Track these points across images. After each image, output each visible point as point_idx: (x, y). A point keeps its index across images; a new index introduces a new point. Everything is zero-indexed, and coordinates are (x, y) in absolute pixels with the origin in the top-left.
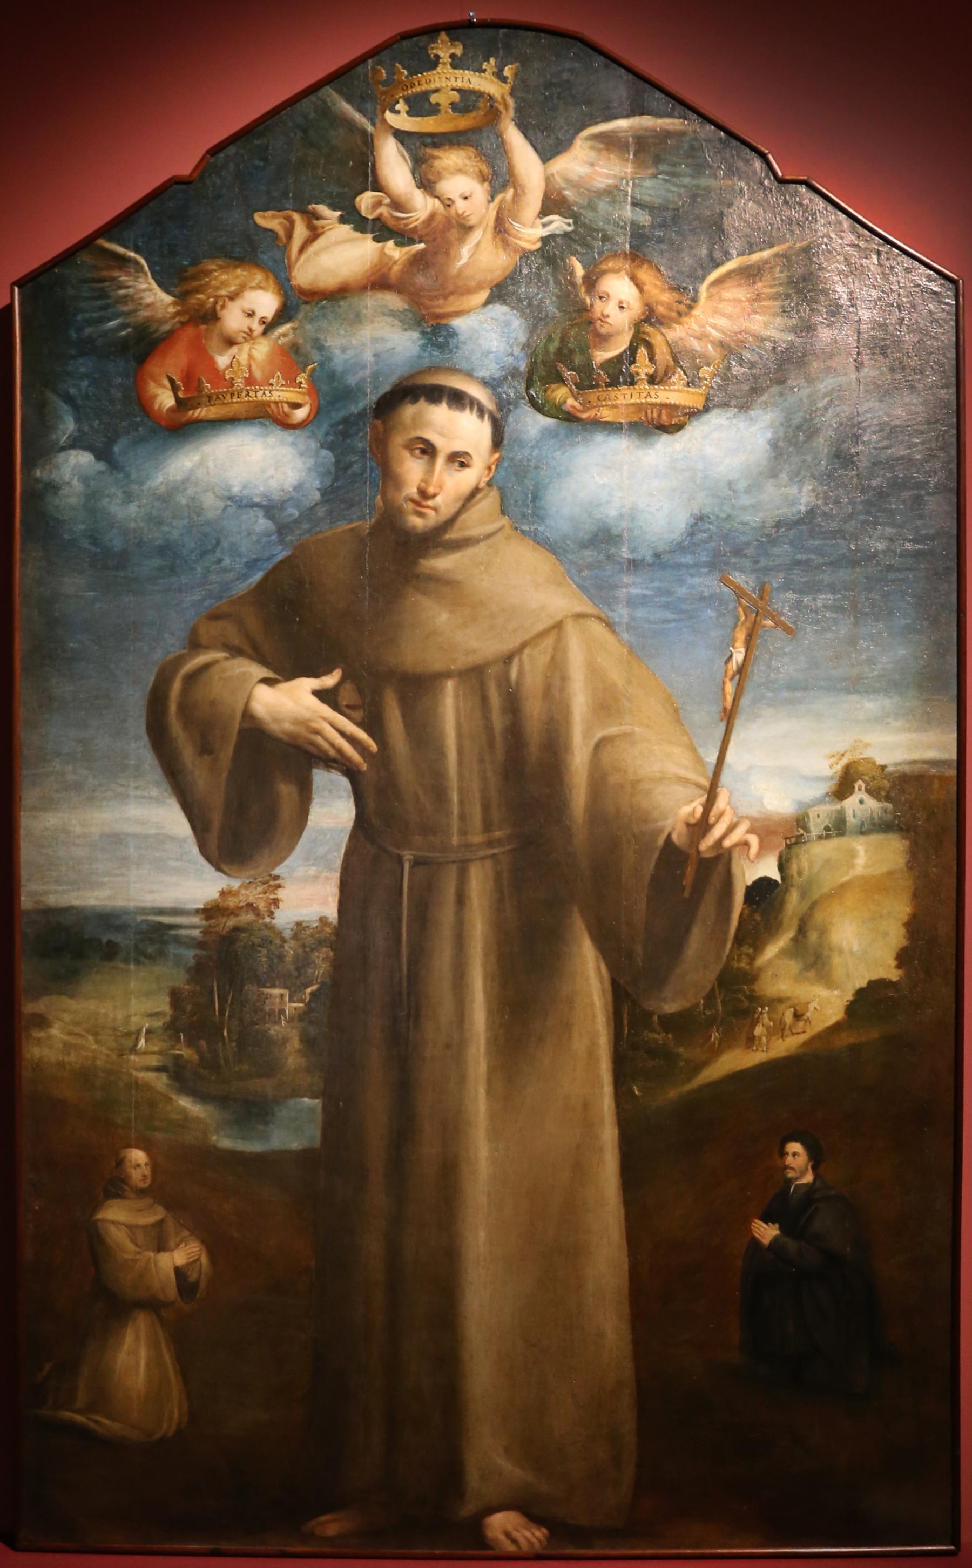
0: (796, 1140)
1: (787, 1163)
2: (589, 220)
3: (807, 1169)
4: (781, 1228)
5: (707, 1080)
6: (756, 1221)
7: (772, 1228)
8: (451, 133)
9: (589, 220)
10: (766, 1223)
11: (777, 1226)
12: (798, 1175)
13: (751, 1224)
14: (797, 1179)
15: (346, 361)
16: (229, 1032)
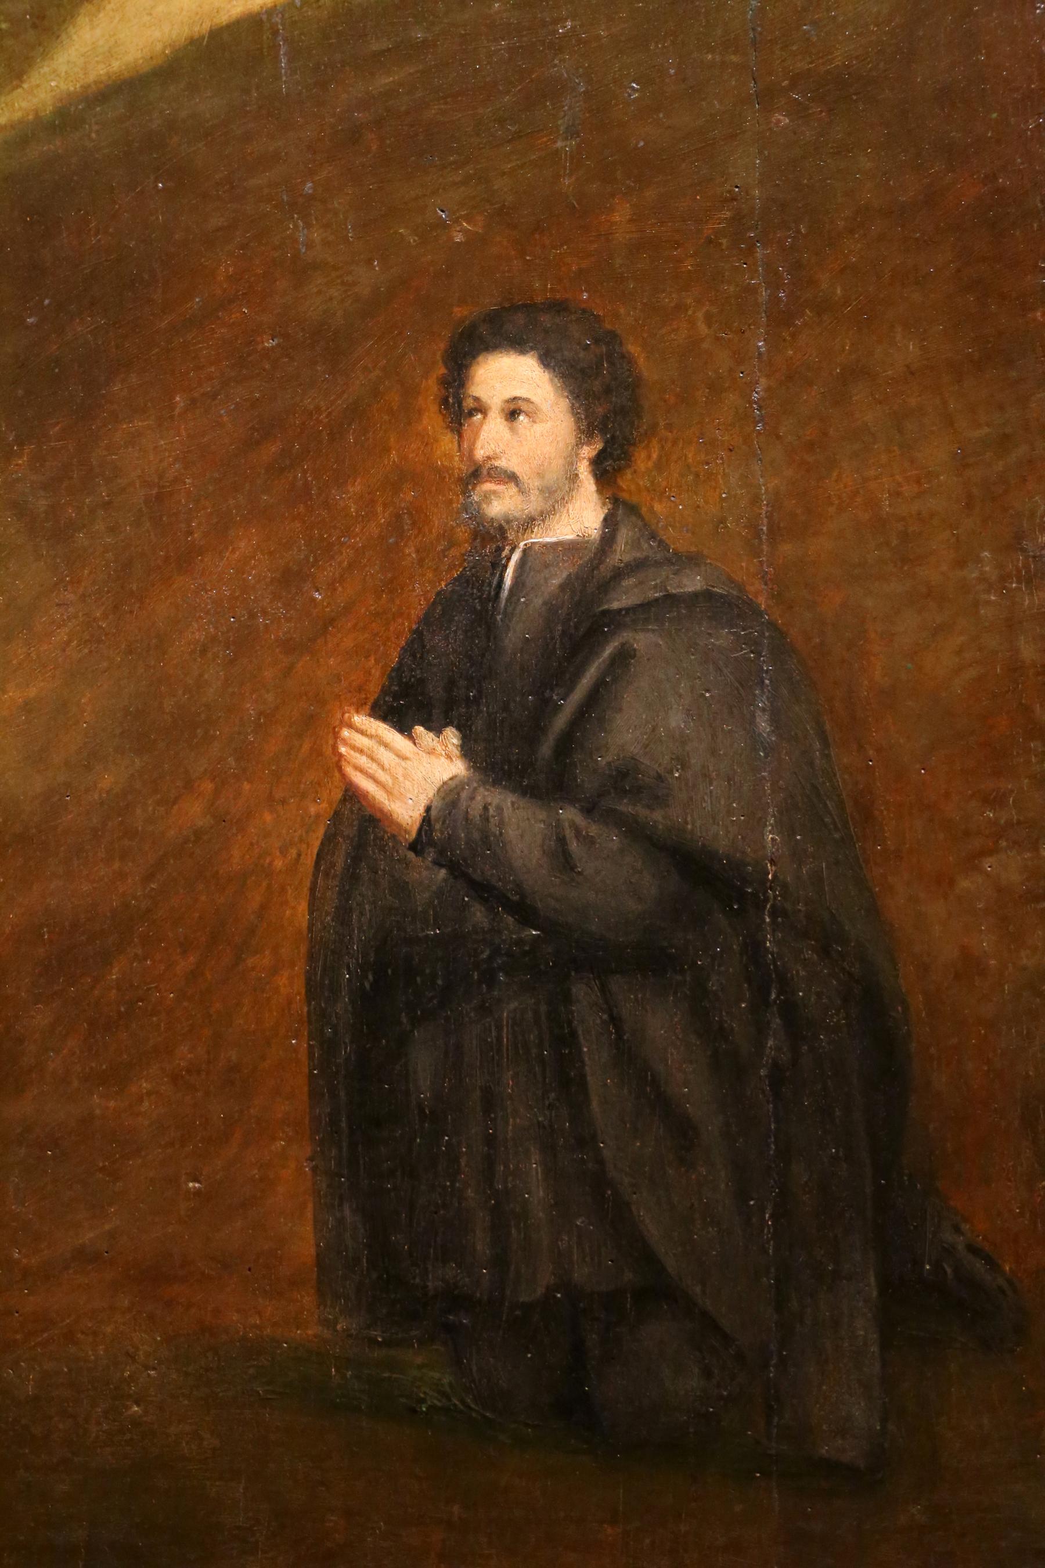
0: (518, 344)
1: (480, 454)
2: (506, 18)
3: (573, 478)
4: (467, 751)
5: (99, 71)
6: (361, 720)
7: (431, 752)
8: (641, 605)
9: (506, 18)
10: (404, 728)
11: (452, 736)
12: (534, 504)
13: (336, 735)
14: (529, 523)
15: (609, 764)
16: (509, 1084)
